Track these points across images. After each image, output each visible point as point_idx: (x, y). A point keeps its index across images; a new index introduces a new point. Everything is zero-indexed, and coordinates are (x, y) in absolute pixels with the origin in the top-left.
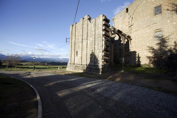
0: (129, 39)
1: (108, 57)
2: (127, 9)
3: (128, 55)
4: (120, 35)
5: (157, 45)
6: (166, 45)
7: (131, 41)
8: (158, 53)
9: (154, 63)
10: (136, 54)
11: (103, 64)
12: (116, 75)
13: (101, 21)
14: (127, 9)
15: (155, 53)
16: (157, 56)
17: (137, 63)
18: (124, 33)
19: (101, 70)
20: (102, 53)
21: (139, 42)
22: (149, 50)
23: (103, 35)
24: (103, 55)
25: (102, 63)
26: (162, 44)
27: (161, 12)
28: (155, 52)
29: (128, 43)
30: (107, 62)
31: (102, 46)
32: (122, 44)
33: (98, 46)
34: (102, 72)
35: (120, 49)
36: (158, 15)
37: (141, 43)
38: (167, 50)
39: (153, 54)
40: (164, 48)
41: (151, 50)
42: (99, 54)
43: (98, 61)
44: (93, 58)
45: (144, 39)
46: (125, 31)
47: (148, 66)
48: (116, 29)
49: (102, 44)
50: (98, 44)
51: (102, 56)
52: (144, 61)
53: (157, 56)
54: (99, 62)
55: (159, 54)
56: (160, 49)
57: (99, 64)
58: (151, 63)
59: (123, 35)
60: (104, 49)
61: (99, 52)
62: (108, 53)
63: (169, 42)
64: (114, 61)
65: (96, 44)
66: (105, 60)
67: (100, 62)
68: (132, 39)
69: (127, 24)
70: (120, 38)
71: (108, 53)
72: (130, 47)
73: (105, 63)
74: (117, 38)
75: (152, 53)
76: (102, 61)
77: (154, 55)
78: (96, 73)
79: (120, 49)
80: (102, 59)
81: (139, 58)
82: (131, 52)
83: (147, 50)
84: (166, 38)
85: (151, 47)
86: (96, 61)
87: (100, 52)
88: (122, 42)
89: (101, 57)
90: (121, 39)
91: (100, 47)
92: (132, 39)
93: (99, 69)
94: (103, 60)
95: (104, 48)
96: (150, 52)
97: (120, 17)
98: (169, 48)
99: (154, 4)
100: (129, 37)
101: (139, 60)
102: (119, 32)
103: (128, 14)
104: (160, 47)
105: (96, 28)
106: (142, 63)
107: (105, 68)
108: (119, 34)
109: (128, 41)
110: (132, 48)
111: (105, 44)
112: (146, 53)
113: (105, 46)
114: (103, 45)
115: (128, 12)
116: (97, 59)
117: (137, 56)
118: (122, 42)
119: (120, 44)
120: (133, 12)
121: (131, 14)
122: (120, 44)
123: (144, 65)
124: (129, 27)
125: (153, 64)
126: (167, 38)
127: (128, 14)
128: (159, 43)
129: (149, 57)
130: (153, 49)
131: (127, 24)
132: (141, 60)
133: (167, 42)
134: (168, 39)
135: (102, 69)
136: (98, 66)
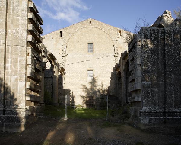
0: (63, 73)
1: (37, 92)
2: (61, 32)
3: (61, 94)
4: (53, 64)
5: (90, 84)
6: (96, 85)
7: (65, 75)
8: (90, 92)
9: (87, 103)
10: (70, 92)
11: (28, 107)
12: (60, 126)
13: (22, 8)
14: (61, 32)
15: (88, 93)
16: (89, 96)
17: (71, 103)
18: (57, 62)
19: (24, 121)
20: (24, 83)
21: (73, 79)
22: (83, 89)
23: (29, 43)
24: (28, 87)
25: (26, 105)
26: (93, 84)
27: (92, 51)
28: (87, 91)
29: (61, 77)
30: (36, 102)
31: (25, 66)
32: (55, 77)
33: (16, 66)
34: (26, 126)
35: (52, 84)
36: (90, 53)
37: (75, 79)
38: (96, 90)
39: (86, 93)
40: (94, 88)
41: (84, 89)
42: (17, 85)
43: (16, 100)
44: (38, 13)
45: (78, 76)
46: (59, 60)
47: (82, 106)
48: (49, 51)
49: (24, 62)
50: (16, 60)
51: (27, 90)
52: (79, 103)
53: (89, 96)
54: (17, 102)
55: (91, 94)
56: (92, 89)
57: (17, 106)
58: (84, 104)
59: (56, 64)
60: (31, 74)
61: (16, 80)
62: (38, 85)
63: (98, 82)
64: (44, 102)
65: (9, 60)
66: (34, 100)
67: (20, 102)
68: (65, 73)
69: (61, 52)
70: (52, 66)
71: (38, 85)
72: (63, 83)
73: (32, 104)
74: (48, 66)
75: (86, 91)
76: (26, 101)
77: (87, 95)
78: (9, 130)
79: (52, 84)
80: (26, 96)
81: (73, 97)
82: (64, 89)
83: (81, 88)
84: (96, 78)
85: (85, 86)
86: (9, 100)
87: (20, 81)
88: (54, 74)
89: (24, 92)
90: (54, 70)
91: (21, 68)
92: (65, 73)
93: (18, 120)
94: (28, 99)
95: (30, 71)
96: (83, 91)
97: (52, 39)
98: (98, 88)
99: (88, 40)
100: (63, 69)
101: (73, 100)
102: (52, 58)
103: (62, 40)
104: (92, 86)
105: (9, 20)
106: (76, 104)
107: (32, 115)
108: (52, 61)
109: (61, 75)
110: (66, 86)
111: (32, 62)
112: (79, 92)
113: (34, 67)
114: (27, 65)
115: (61, 36)
116: (12, 97)
117: (71, 95)
118: (54, 74)
119: (53, 77)
120: (68, 39)
121: (65, 41)
122: (52, 76)
123: (78, 107)
124: (63, 57)
125: (87, 105)
126: (96, 79)
127: (62, 40)
128: (90, 83)
129: (83, 97)
130: (86, 88)
131: (61, 52)
132: (75, 99)
133: (96, 82)
134: (97, 79)
135: (27, 117)
136: (15, 112)
